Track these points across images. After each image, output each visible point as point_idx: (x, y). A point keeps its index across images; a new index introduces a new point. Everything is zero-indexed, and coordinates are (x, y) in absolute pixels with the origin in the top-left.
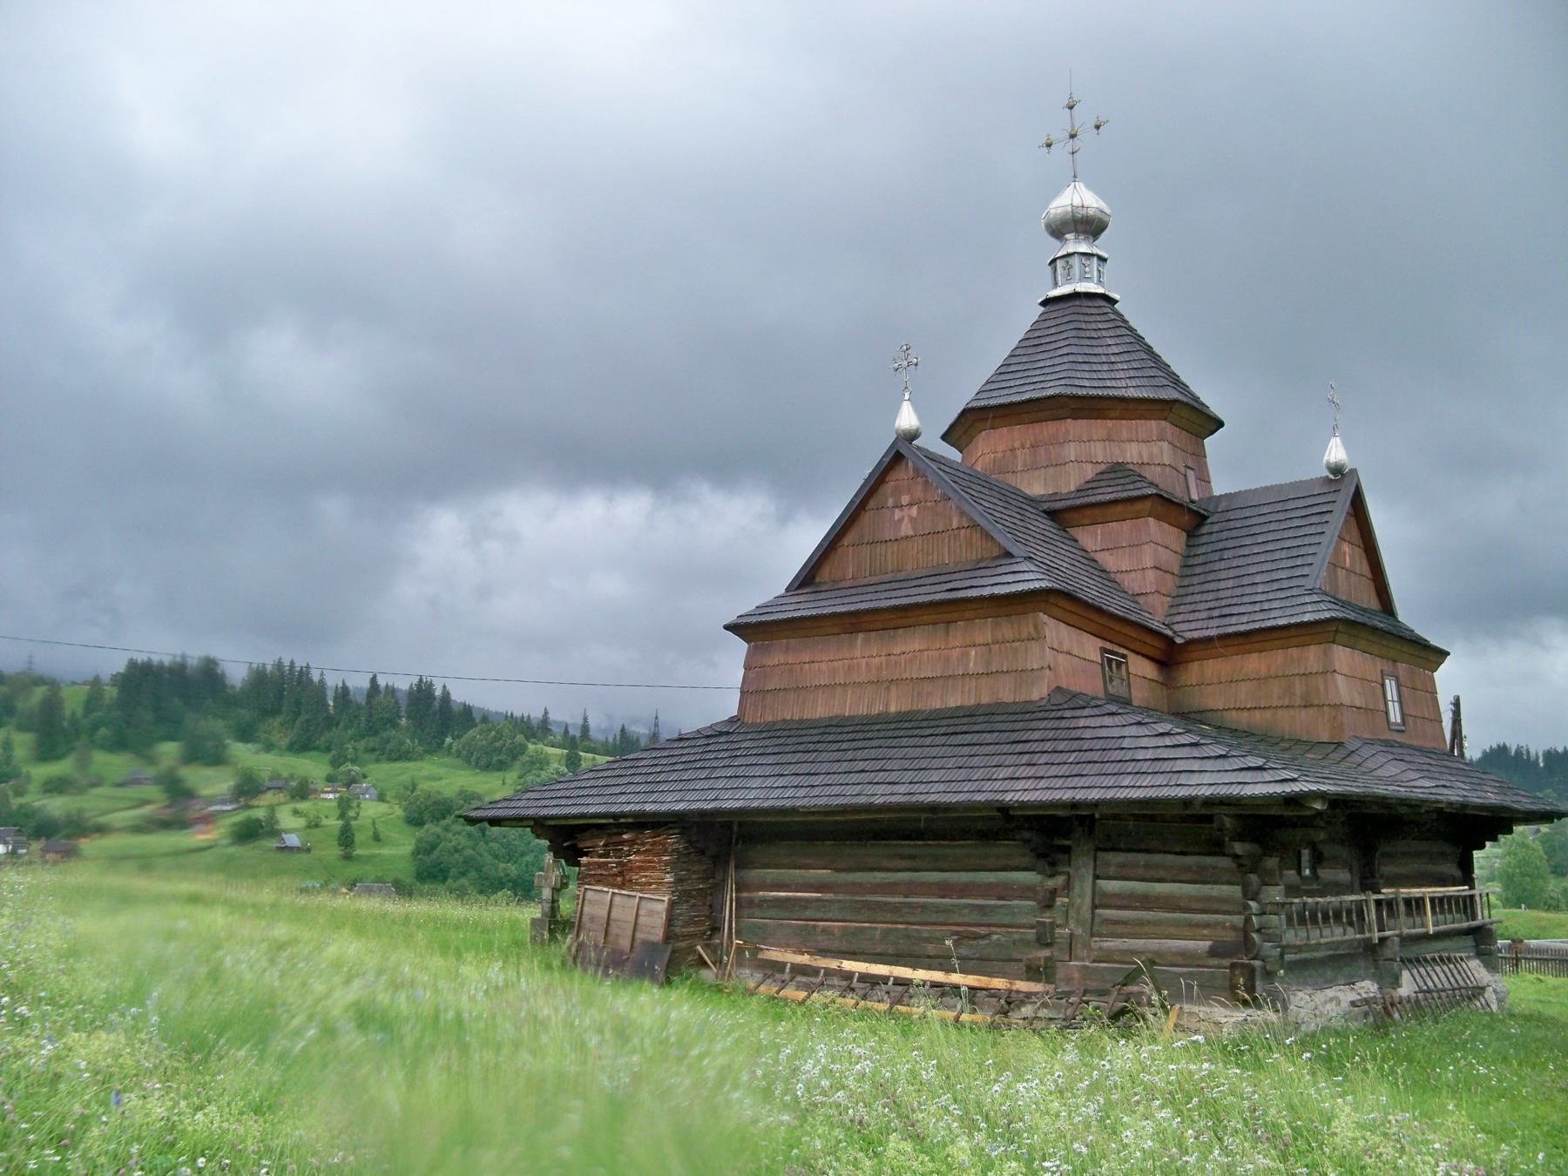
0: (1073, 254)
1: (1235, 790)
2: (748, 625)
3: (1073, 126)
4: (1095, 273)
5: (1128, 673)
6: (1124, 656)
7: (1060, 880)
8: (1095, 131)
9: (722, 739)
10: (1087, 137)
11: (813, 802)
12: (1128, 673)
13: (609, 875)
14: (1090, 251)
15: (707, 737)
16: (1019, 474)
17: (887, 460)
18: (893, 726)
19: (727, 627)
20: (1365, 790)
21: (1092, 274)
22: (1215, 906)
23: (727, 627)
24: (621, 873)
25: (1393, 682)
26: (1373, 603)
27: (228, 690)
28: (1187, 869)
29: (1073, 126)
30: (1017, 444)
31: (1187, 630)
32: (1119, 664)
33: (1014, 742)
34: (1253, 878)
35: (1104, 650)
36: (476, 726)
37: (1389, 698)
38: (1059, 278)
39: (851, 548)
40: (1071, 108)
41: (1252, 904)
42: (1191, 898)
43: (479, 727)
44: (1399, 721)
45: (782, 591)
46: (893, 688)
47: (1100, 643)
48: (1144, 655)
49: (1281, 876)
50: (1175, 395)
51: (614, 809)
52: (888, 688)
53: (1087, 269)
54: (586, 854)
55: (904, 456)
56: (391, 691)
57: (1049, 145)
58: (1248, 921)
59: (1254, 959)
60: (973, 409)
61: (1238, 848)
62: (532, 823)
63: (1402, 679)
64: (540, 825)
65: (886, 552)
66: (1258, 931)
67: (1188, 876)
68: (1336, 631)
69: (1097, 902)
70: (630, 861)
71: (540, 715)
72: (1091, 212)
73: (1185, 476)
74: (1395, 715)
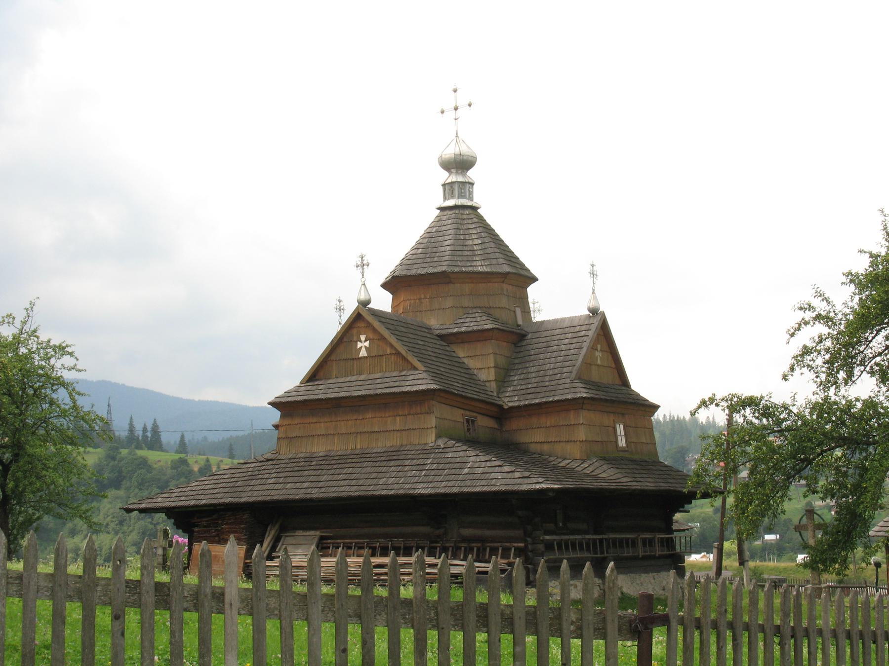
0: (455, 182)
1: (516, 488)
2: (281, 403)
4: (467, 193)
7: (442, 531)
9: (270, 463)
13: (211, 537)
14: (464, 181)
16: (423, 312)
17: (354, 316)
18: (358, 456)
20: (575, 486)
21: (466, 194)
24: (218, 535)
25: (622, 426)
27: (155, 466)
30: (422, 296)
31: (510, 400)
33: (418, 465)
34: (529, 528)
37: (619, 433)
38: (447, 195)
40: (455, 91)
41: (529, 539)
45: (298, 384)
46: (359, 436)
47: (462, 411)
48: (487, 416)
50: (506, 269)
52: (356, 437)
53: (463, 191)
54: (197, 526)
61: (520, 513)
64: (170, 512)
65: (353, 365)
66: (532, 551)
68: (583, 403)
70: (222, 528)
72: (465, 158)
73: (515, 312)
74: (622, 442)
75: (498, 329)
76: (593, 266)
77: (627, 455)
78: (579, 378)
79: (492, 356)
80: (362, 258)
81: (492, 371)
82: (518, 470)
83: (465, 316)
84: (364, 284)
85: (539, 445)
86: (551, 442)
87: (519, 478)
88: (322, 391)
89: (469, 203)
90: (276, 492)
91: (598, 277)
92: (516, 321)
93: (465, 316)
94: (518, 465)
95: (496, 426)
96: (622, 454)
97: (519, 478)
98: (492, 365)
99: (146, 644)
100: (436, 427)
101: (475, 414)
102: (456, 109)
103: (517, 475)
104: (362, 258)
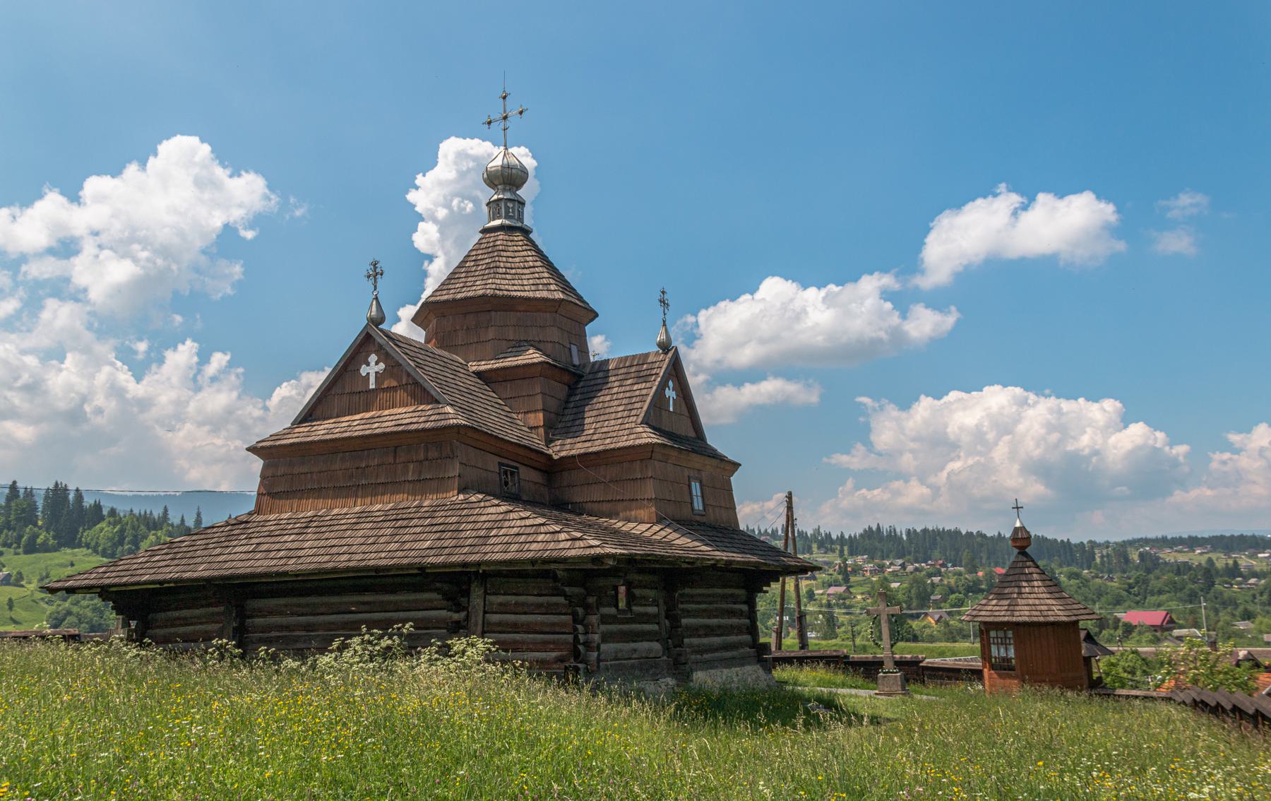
3: (505, 111)
5: (519, 479)
6: (517, 468)
8: (519, 115)
10: (514, 120)
11: (299, 567)
12: (519, 479)
15: (232, 525)
19: (248, 449)
22: (557, 629)
23: (248, 449)
25: (697, 484)
26: (692, 434)
28: (540, 605)
29: (505, 111)
32: (512, 473)
35: (500, 464)
36: (104, 519)
37: (694, 493)
39: (337, 397)
40: (504, 98)
42: (542, 624)
43: (107, 520)
44: (701, 508)
49: (598, 609)
51: (160, 577)
55: (805, 289)
56: (29, 493)
57: (489, 123)
58: (576, 638)
59: (581, 662)
60: (432, 303)
62: (99, 590)
63: (704, 483)
64: (104, 592)
66: (583, 644)
67: (543, 610)
69: (485, 629)
71: (996, 534)
74: (698, 505)
75: (548, 363)
76: (663, 292)
77: (704, 520)
78: (647, 424)
79: (540, 397)
80: (375, 265)
81: (541, 415)
82: (566, 530)
83: (510, 350)
84: (376, 298)
85: (596, 504)
86: (612, 500)
87: (567, 540)
88: (322, 430)
89: (519, 224)
90: (240, 564)
91: (669, 308)
92: (572, 361)
93: (510, 350)
94: (567, 525)
95: (540, 481)
96: (698, 518)
97: (567, 540)
98: (540, 406)
99: (499, 629)
100: (459, 476)
101: (518, 465)
102: (505, 118)
103: (563, 536)
104: (375, 265)
